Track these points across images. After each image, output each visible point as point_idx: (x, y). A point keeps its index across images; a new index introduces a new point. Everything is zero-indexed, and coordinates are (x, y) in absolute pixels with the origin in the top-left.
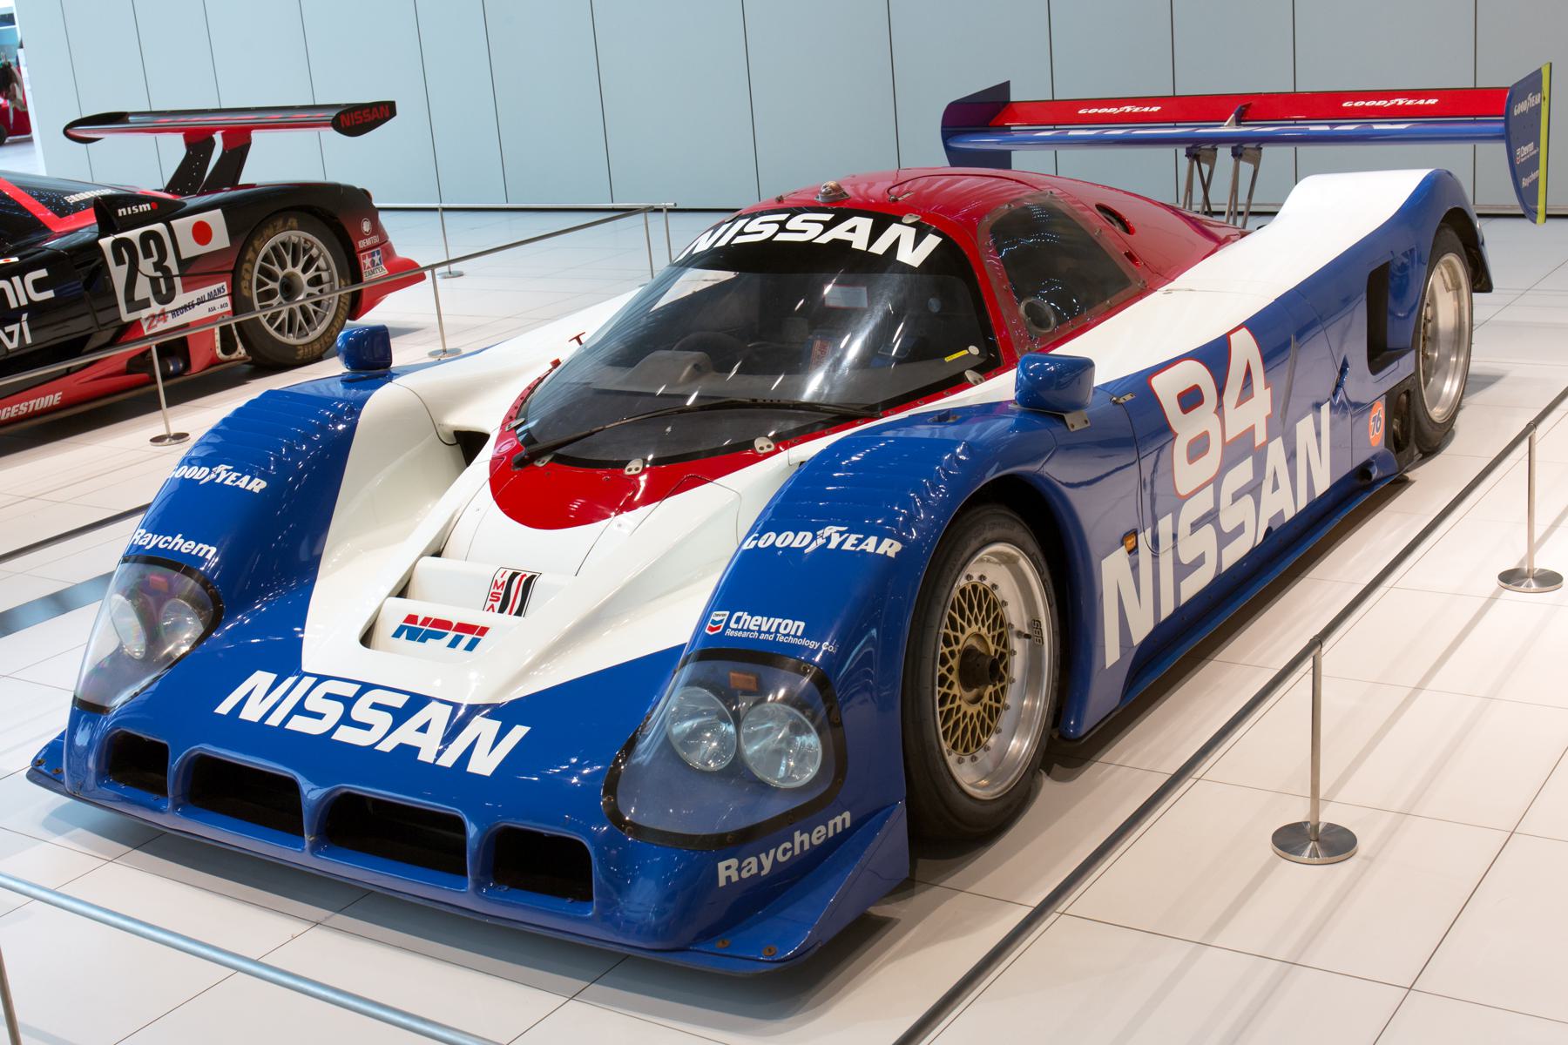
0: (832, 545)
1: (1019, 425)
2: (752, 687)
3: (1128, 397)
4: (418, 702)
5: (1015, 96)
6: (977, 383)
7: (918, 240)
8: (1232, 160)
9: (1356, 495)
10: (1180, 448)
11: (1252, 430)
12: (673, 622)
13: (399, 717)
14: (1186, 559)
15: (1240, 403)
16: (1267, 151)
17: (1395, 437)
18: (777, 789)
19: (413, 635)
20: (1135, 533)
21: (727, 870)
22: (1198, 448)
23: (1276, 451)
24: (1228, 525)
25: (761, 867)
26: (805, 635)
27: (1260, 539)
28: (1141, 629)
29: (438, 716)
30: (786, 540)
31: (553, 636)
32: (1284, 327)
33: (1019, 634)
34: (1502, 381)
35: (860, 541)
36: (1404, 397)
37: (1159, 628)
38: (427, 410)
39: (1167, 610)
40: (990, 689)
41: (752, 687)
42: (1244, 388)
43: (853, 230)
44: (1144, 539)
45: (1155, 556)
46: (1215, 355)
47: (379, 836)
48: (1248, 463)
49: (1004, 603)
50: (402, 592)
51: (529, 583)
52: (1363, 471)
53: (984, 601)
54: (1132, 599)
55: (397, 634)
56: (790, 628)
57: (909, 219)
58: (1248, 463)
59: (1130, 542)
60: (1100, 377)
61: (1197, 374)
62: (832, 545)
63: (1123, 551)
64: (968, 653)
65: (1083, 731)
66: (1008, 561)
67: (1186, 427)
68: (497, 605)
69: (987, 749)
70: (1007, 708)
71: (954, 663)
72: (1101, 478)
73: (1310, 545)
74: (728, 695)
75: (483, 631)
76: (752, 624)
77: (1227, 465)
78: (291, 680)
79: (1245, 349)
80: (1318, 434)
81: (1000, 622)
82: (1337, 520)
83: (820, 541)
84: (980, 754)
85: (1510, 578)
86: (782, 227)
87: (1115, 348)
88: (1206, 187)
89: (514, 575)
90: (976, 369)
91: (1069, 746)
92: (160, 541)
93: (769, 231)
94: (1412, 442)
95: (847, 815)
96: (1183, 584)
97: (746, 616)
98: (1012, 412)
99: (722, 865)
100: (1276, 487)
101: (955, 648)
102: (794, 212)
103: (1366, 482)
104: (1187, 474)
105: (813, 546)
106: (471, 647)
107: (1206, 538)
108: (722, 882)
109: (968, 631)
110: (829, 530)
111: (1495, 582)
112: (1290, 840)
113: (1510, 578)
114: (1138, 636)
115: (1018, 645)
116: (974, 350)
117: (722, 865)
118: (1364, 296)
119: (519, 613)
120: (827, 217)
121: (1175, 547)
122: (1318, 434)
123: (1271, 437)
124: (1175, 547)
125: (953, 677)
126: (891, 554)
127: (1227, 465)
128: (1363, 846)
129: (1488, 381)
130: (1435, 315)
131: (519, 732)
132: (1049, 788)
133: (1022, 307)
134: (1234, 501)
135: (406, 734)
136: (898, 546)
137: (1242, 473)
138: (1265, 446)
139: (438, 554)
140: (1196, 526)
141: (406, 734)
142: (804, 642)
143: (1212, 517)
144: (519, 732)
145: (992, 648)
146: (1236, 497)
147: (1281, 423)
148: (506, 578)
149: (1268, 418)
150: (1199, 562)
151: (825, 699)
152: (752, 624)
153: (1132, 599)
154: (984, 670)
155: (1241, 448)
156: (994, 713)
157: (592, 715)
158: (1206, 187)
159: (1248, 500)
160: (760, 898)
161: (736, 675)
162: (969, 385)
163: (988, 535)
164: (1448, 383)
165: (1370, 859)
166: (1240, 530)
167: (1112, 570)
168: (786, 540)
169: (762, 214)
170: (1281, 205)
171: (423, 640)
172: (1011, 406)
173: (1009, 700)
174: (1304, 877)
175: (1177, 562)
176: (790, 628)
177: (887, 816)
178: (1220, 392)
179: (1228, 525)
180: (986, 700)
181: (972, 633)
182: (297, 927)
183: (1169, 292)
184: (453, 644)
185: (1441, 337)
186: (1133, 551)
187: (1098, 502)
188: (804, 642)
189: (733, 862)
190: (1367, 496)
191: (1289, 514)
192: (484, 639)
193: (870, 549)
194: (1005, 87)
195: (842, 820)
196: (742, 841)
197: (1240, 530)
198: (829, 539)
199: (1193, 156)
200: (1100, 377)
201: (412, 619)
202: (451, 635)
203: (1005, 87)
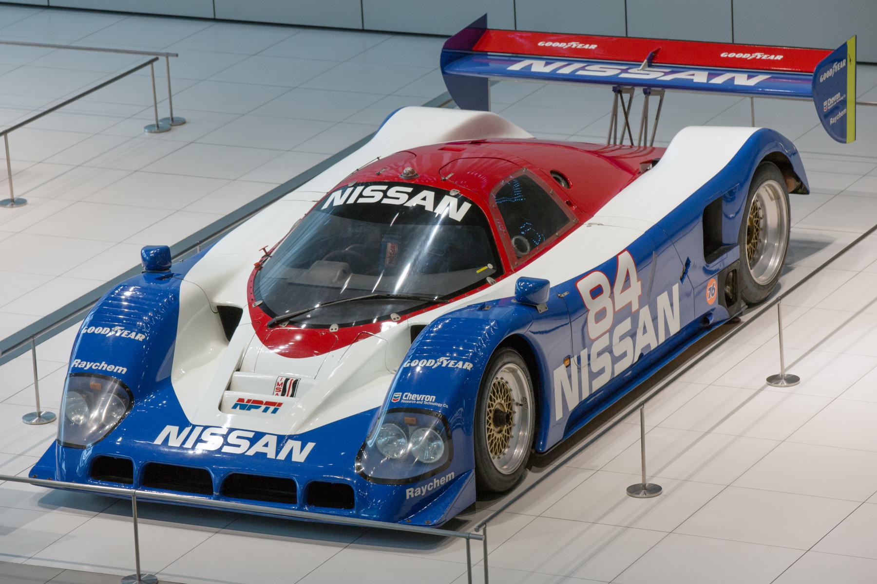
0: (444, 365)
1: (516, 311)
2: (414, 423)
3: (566, 294)
4: (258, 436)
5: (490, 25)
6: (493, 284)
7: (459, 206)
8: (643, 96)
9: (698, 336)
10: (591, 317)
11: (630, 303)
12: (375, 394)
13: (253, 441)
14: (595, 369)
15: (623, 290)
16: (668, 93)
17: (727, 295)
18: (425, 464)
19: (243, 407)
20: (569, 357)
21: (410, 493)
22: (601, 315)
23: (645, 315)
24: (617, 353)
25: (422, 492)
26: (436, 401)
27: (636, 359)
28: (573, 403)
29: (273, 441)
30: (99, 330)
31: (319, 402)
32: (645, 249)
33: (517, 404)
34: (828, 248)
35: (456, 363)
36: (731, 274)
37: (582, 403)
38: (205, 295)
39: (586, 394)
40: (505, 428)
41: (414, 423)
42: (625, 281)
43: (424, 199)
44: (574, 361)
45: (579, 369)
46: (610, 268)
47: (252, 493)
48: (629, 320)
49: (511, 390)
50: (228, 388)
51: (295, 384)
52: (705, 318)
53: (502, 389)
54: (568, 390)
55: (235, 407)
56: (429, 399)
57: (453, 193)
58: (629, 320)
59: (567, 363)
60: (552, 285)
61: (599, 278)
62: (444, 365)
63: (563, 366)
64: (496, 411)
65: (547, 448)
66: (513, 371)
67: (593, 306)
68: (280, 393)
69: (504, 454)
70: (512, 437)
71: (491, 415)
72: (558, 327)
73: (668, 362)
74: (403, 426)
75: (280, 404)
76: (411, 398)
77: (617, 322)
78: (187, 430)
79: (626, 262)
80: (672, 305)
81: (509, 398)
82: (686, 348)
83: (439, 364)
84: (501, 456)
85: (773, 380)
86: (385, 196)
87: (559, 263)
88: (626, 115)
89: (287, 380)
90: (491, 276)
91: (539, 458)
92: (87, 365)
93: (378, 196)
94: (739, 299)
95: (453, 473)
96: (594, 382)
97: (409, 394)
98: (513, 304)
99: (407, 491)
100: (645, 331)
101: (492, 409)
102: (391, 185)
103: (706, 325)
104: (594, 329)
105: (436, 366)
106: (275, 411)
107: (606, 358)
108: (408, 497)
109: (497, 402)
110: (442, 359)
111: (765, 382)
112: (634, 490)
113: (773, 380)
114: (572, 406)
115: (516, 409)
116: (490, 266)
117: (407, 491)
118: (701, 219)
119: (292, 396)
120: (410, 190)
121: (589, 364)
122: (672, 305)
123: (641, 306)
124: (589, 364)
125: (491, 421)
126: (469, 368)
127: (617, 322)
128: (665, 491)
129: (811, 247)
130: (765, 216)
131: (310, 446)
132: (531, 477)
133: (513, 241)
134: (620, 340)
135: (258, 447)
136: (471, 365)
137: (626, 326)
138: (638, 311)
139: (238, 370)
140: (599, 354)
141: (258, 447)
142: (436, 404)
143: (609, 349)
144: (310, 446)
145: (506, 410)
146: (622, 338)
147: (648, 298)
148: (283, 381)
149: (640, 297)
150: (602, 371)
151: (446, 429)
152: (411, 398)
153: (568, 390)
154: (502, 419)
155: (625, 313)
156: (507, 439)
157: (344, 437)
158: (626, 115)
159: (629, 340)
160: (420, 504)
161: (408, 418)
162: (489, 285)
163: (506, 360)
164: (772, 260)
165: (666, 496)
166: (624, 355)
167: (558, 376)
168: (99, 330)
169: (371, 185)
170: (669, 142)
171: (249, 409)
172: (513, 301)
173: (513, 433)
174: (639, 503)
175: (590, 372)
176: (429, 399)
177: (466, 477)
178: (612, 283)
179: (617, 353)
180: (504, 432)
181: (498, 403)
182: (211, 534)
183: (590, 225)
184: (265, 410)
185: (769, 230)
186: (568, 366)
187: (551, 344)
188: (436, 404)
189: (412, 489)
190: (707, 333)
191: (654, 346)
192: (281, 409)
193: (133, 337)
194: (484, 18)
195: (451, 475)
196: (414, 482)
197: (624, 355)
198: (442, 363)
199: (618, 91)
200: (552, 285)
201: (241, 400)
202: (263, 407)
203: (484, 18)
